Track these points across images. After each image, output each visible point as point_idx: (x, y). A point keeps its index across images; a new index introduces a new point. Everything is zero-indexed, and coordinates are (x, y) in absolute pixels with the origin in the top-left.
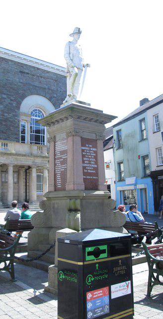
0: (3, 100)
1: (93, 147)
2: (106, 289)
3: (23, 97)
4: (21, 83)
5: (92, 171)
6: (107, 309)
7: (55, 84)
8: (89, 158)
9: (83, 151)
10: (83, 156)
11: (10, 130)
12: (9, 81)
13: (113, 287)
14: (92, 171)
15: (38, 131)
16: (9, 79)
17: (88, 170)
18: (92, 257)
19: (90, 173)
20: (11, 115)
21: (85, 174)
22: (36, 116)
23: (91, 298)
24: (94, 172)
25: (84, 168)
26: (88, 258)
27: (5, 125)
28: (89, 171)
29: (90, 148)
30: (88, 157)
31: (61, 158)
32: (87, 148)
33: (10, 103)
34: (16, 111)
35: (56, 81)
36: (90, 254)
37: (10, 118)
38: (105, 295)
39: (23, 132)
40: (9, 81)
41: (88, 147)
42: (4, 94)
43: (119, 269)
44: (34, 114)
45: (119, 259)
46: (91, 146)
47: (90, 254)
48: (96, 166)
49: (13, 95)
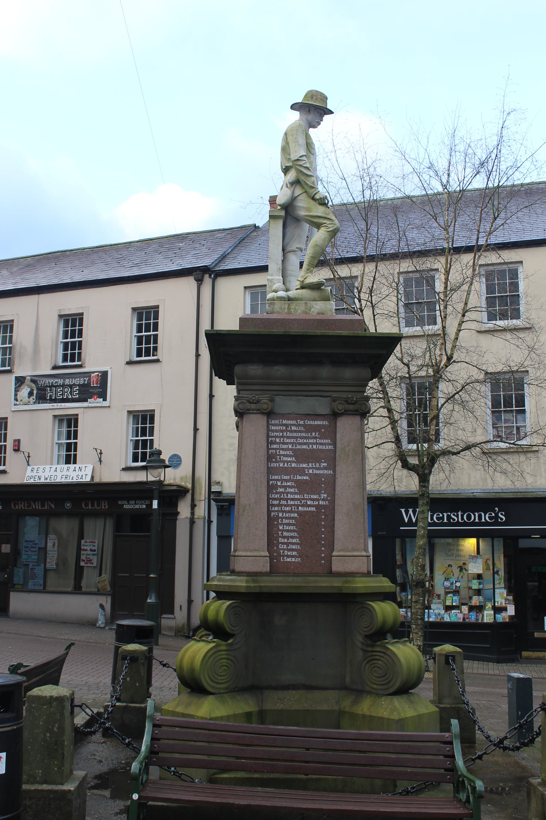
31: (302, 472)
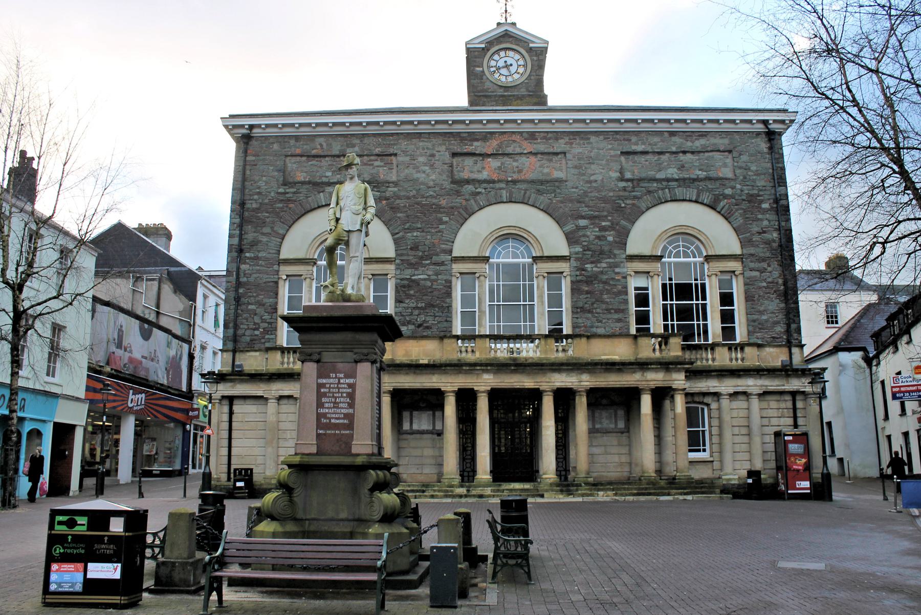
0: (581, 233)
1: (346, 377)
2: (80, 566)
3: (635, 214)
4: (628, 180)
5: (341, 421)
6: (79, 588)
7: (729, 161)
8: (336, 398)
9: (320, 386)
10: (320, 395)
11: (603, 302)
12: (594, 185)
13: (91, 566)
14: (341, 421)
15: (684, 291)
16: (592, 178)
17: (330, 419)
18: (64, 528)
19: (335, 424)
20: (604, 265)
21: (319, 425)
22: (677, 255)
23: (57, 571)
24: (345, 421)
25: (319, 416)
26: (57, 527)
27: (587, 292)
28: (333, 421)
29: (339, 379)
30: (333, 397)
32: (331, 381)
33: (598, 238)
34: (616, 252)
35: (730, 152)
36: (60, 523)
37: (602, 272)
38: (77, 571)
39: (642, 299)
40: (594, 185)
41: (336, 377)
42: (583, 218)
43: (103, 546)
44: (671, 252)
45: (105, 536)
46: (342, 375)
47: (60, 523)
48: (351, 411)
49: (606, 216)
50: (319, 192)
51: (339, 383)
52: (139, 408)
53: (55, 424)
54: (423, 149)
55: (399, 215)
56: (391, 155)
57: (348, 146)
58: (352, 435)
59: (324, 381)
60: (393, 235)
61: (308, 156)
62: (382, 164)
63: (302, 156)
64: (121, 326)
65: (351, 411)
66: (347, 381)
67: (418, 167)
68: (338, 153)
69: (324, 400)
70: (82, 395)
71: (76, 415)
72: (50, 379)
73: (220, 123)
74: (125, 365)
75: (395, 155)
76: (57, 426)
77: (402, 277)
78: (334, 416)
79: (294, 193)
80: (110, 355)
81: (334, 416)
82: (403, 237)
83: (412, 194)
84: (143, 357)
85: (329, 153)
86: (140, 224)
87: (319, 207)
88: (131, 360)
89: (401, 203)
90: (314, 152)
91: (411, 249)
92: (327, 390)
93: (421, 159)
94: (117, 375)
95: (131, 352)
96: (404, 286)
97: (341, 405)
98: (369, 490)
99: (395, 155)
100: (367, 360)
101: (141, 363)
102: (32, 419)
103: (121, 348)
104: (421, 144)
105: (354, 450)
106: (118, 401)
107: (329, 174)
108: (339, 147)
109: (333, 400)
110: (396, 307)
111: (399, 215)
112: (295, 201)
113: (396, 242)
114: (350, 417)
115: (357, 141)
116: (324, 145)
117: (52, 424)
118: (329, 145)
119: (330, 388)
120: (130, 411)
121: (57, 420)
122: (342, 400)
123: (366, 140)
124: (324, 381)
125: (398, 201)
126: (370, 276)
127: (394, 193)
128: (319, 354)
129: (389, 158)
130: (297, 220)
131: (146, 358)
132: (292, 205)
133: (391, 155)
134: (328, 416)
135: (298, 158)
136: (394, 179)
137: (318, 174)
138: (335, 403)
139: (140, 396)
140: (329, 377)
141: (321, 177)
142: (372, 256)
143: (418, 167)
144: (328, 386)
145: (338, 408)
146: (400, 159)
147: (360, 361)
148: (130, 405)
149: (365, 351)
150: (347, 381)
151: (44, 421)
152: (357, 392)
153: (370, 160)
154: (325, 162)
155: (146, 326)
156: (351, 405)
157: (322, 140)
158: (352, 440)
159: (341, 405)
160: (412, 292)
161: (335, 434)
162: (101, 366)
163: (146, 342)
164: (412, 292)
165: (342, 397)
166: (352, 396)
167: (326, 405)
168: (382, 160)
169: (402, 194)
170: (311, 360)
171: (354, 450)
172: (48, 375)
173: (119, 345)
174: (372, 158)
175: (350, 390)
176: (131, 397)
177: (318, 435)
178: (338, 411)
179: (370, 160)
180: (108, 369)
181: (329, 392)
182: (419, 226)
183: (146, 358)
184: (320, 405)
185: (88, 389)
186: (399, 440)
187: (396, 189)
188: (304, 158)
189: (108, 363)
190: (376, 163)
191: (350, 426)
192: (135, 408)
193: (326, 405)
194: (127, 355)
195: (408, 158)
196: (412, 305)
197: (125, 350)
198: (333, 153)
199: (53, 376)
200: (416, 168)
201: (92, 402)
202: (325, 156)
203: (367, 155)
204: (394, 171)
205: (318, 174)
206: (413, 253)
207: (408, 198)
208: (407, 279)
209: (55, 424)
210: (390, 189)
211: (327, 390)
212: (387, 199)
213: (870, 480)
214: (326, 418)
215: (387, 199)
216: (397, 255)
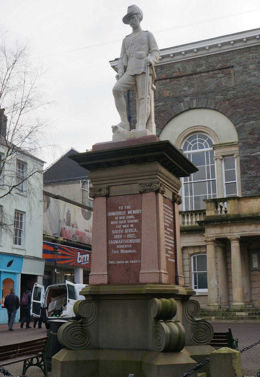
1: (133, 209)
5: (130, 251)
8: (124, 229)
14: (130, 251)
17: (119, 249)
25: (109, 247)
28: (122, 251)
29: (127, 210)
32: (120, 213)
41: (124, 210)
48: (138, 241)
50: (180, 103)
51: (127, 214)
52: (85, 263)
53: (22, 274)
54: (253, 59)
55: (238, 110)
56: (229, 68)
57: (197, 66)
58: (140, 264)
59: (114, 214)
60: (235, 125)
61: (170, 78)
62: (223, 75)
63: (166, 79)
64: (69, 211)
65: (138, 241)
66: (134, 212)
67: (250, 73)
68: (191, 72)
69: (113, 232)
70: (40, 254)
71: (37, 269)
72: (17, 246)
73: (109, 65)
74: (73, 236)
75: (232, 67)
76: (23, 276)
77: (245, 155)
78: (122, 246)
79: (163, 105)
80: (62, 230)
81: (122, 246)
82: (243, 126)
83: (246, 93)
84: (86, 230)
85: (185, 74)
86: (87, 150)
87: (181, 113)
88: (78, 233)
89: (240, 101)
90: (174, 75)
91: (250, 134)
92: (116, 222)
93: (251, 67)
94: (68, 243)
95: (77, 227)
96: (246, 161)
97: (129, 236)
98: (155, 318)
99: (232, 67)
100: (151, 190)
101: (85, 234)
102: (5, 272)
103: (70, 226)
104: (251, 55)
105: (142, 280)
106: (68, 259)
107: (186, 89)
108: (191, 69)
109: (122, 231)
110: (241, 177)
111: (238, 110)
112: (164, 111)
113: (239, 130)
114: (137, 247)
115: (204, 62)
116: (181, 68)
117: (20, 274)
118: (184, 68)
119: (119, 220)
120: (80, 266)
121: (23, 272)
122: (130, 230)
123: (210, 60)
124: (114, 214)
125: (237, 100)
126: (221, 157)
127: (234, 95)
128: (108, 188)
129: (228, 70)
130: (166, 124)
131: (88, 231)
132: (162, 114)
133: (229, 68)
134: (118, 247)
135: (164, 81)
136: (233, 84)
137: (178, 90)
138: (123, 234)
139: (85, 256)
140: (118, 210)
141: (180, 92)
142: (221, 143)
143: (250, 73)
144: (116, 218)
145: (126, 238)
146: (236, 69)
147: (145, 191)
148: (79, 262)
149: (149, 181)
150: (134, 212)
151: (14, 273)
152: (143, 222)
153: (215, 74)
154: (182, 81)
155: (86, 210)
156: (138, 235)
157: (178, 65)
158: (140, 270)
159: (129, 236)
160: (252, 166)
161: (124, 264)
162: (56, 238)
163: (86, 221)
164: (252, 166)
165: (130, 228)
166: (138, 226)
167: (116, 237)
168: (223, 73)
169: (239, 94)
170: (101, 196)
171: (142, 280)
172: (16, 243)
173: (68, 224)
174: (216, 72)
175: (136, 221)
176: (79, 256)
177: (109, 266)
178: (127, 241)
179: (215, 74)
180: (61, 239)
181: (118, 224)
182: (254, 116)
183: (88, 231)
184: (110, 237)
185: (45, 251)
186: (250, 275)
187: (235, 92)
188: (168, 80)
189: (61, 235)
190: (219, 75)
191: (138, 255)
192: (82, 264)
193: (116, 237)
194: (74, 229)
195: (241, 68)
196: (253, 175)
197: (73, 226)
198: (188, 73)
199: (20, 244)
200: (248, 74)
201: (47, 260)
202: (182, 76)
203: (212, 71)
204: (232, 79)
205: (178, 90)
206: (251, 136)
207: (245, 97)
208: (248, 156)
209: (22, 274)
210: (230, 92)
211: (116, 222)
212: (228, 100)
213: (8, 331)
214: (116, 249)
215: (228, 100)
216: (239, 139)
